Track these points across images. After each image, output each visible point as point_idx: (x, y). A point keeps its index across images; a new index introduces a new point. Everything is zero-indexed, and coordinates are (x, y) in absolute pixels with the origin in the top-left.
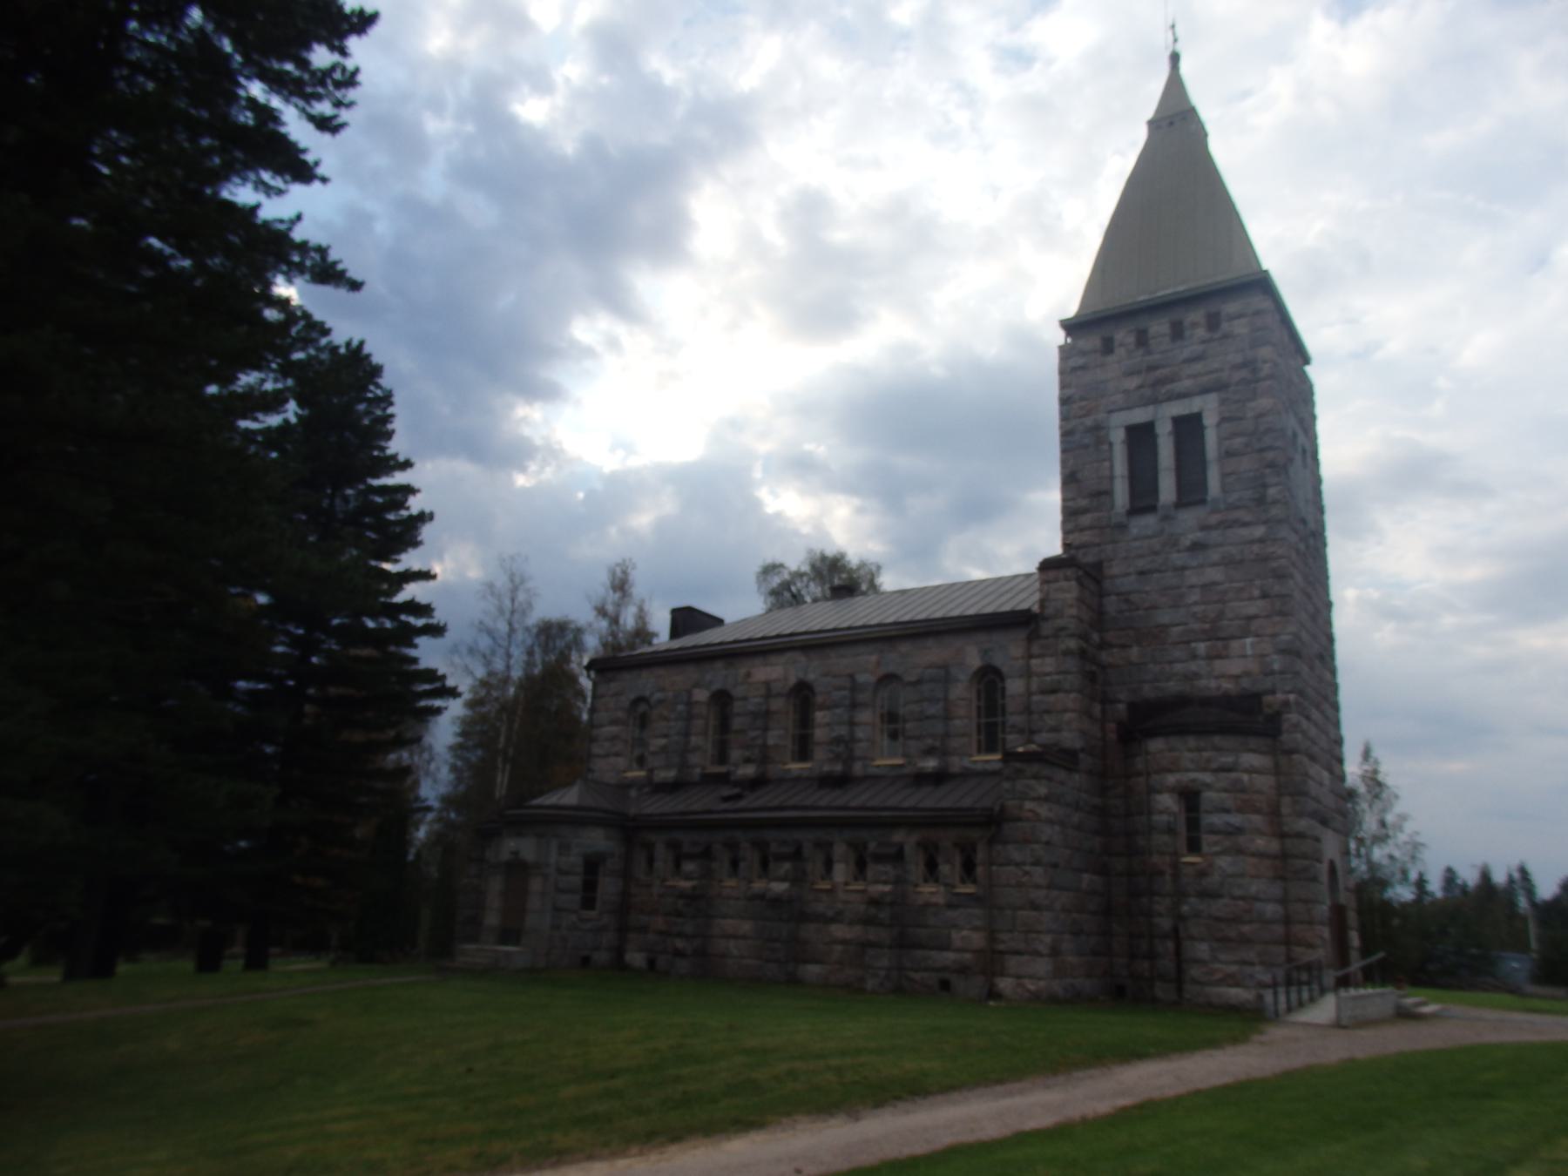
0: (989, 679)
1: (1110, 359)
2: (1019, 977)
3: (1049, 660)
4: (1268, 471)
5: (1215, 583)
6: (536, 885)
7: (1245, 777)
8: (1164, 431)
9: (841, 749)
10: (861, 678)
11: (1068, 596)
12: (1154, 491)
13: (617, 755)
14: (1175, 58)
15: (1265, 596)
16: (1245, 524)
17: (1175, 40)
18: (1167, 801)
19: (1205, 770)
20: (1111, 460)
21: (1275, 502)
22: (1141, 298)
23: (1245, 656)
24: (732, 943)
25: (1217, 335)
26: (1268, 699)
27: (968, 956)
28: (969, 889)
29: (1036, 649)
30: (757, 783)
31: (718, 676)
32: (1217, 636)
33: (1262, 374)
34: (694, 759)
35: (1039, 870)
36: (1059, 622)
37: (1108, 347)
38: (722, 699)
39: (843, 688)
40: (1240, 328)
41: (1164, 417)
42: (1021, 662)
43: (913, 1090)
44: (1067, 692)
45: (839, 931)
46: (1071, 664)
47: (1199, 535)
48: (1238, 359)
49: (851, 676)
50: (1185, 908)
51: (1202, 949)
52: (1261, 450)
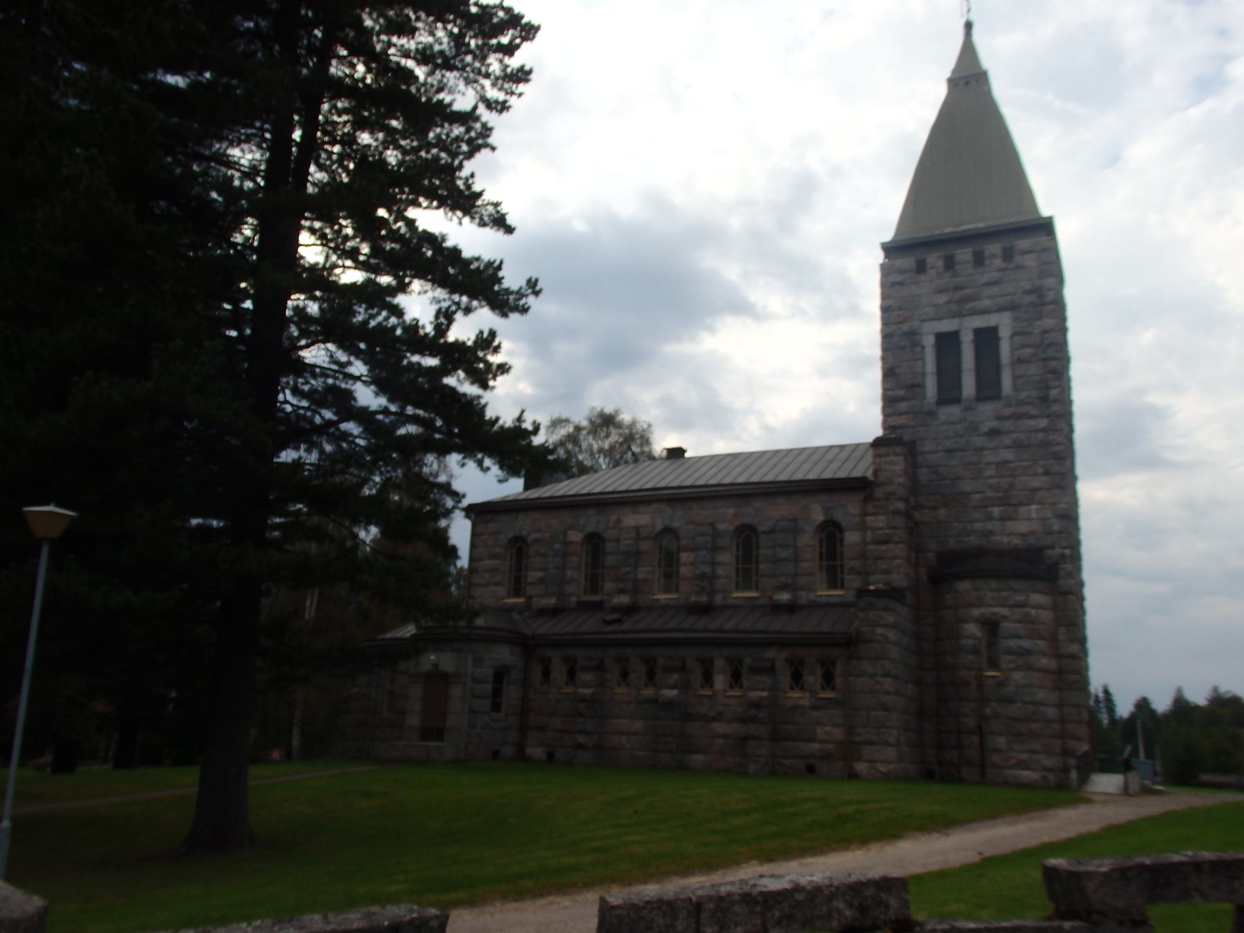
0: (831, 532)
1: (923, 277)
2: (872, 761)
3: (880, 517)
4: (1050, 376)
5: (1006, 462)
6: (456, 691)
7: (1033, 612)
8: (967, 339)
9: (706, 583)
10: (721, 527)
11: (896, 468)
12: (958, 386)
13: (497, 584)
14: (969, 26)
15: (1046, 473)
16: (1032, 417)
17: (969, 10)
18: (972, 628)
19: (1003, 606)
20: (923, 359)
21: (1056, 401)
22: (947, 230)
23: (1030, 519)
24: (624, 738)
25: (1011, 266)
26: (1049, 552)
27: (830, 746)
28: (830, 695)
29: (870, 509)
30: (631, 610)
31: (591, 521)
32: (1010, 503)
33: (1048, 299)
34: (569, 589)
35: (888, 680)
36: (890, 488)
37: (921, 267)
38: (595, 542)
39: (703, 534)
40: (1030, 261)
41: (968, 327)
42: (858, 519)
43: (890, 831)
44: (897, 543)
45: (719, 727)
46: (899, 521)
47: (994, 424)
48: (1027, 285)
49: (712, 525)
50: (988, 711)
51: (1001, 742)
52: (1045, 360)
